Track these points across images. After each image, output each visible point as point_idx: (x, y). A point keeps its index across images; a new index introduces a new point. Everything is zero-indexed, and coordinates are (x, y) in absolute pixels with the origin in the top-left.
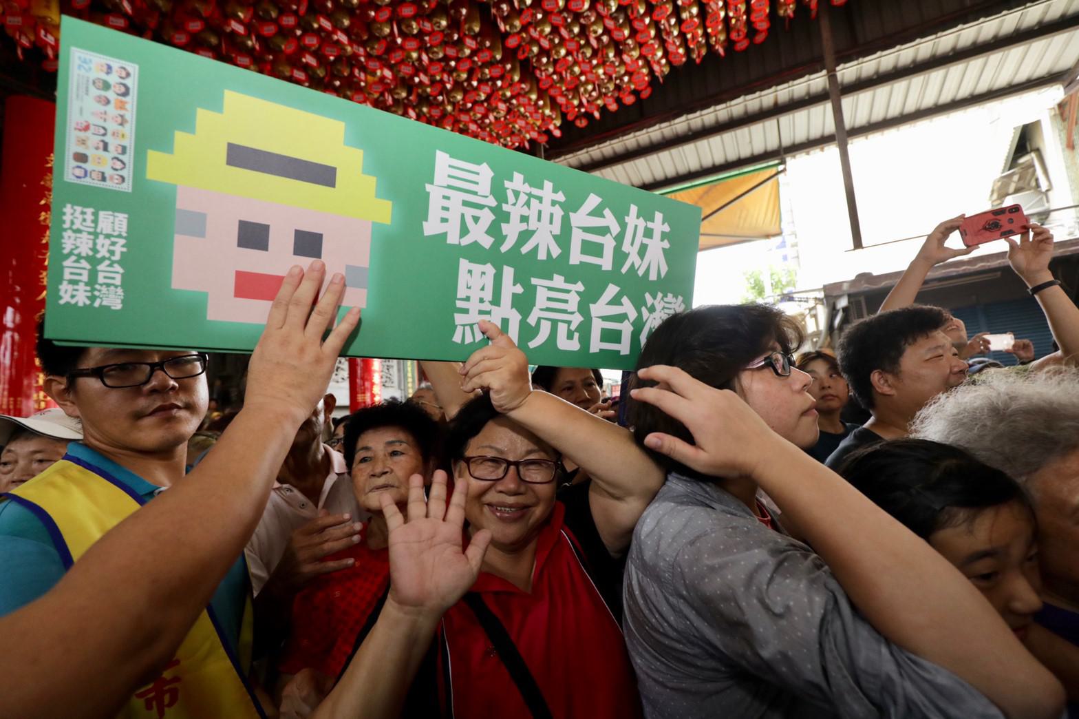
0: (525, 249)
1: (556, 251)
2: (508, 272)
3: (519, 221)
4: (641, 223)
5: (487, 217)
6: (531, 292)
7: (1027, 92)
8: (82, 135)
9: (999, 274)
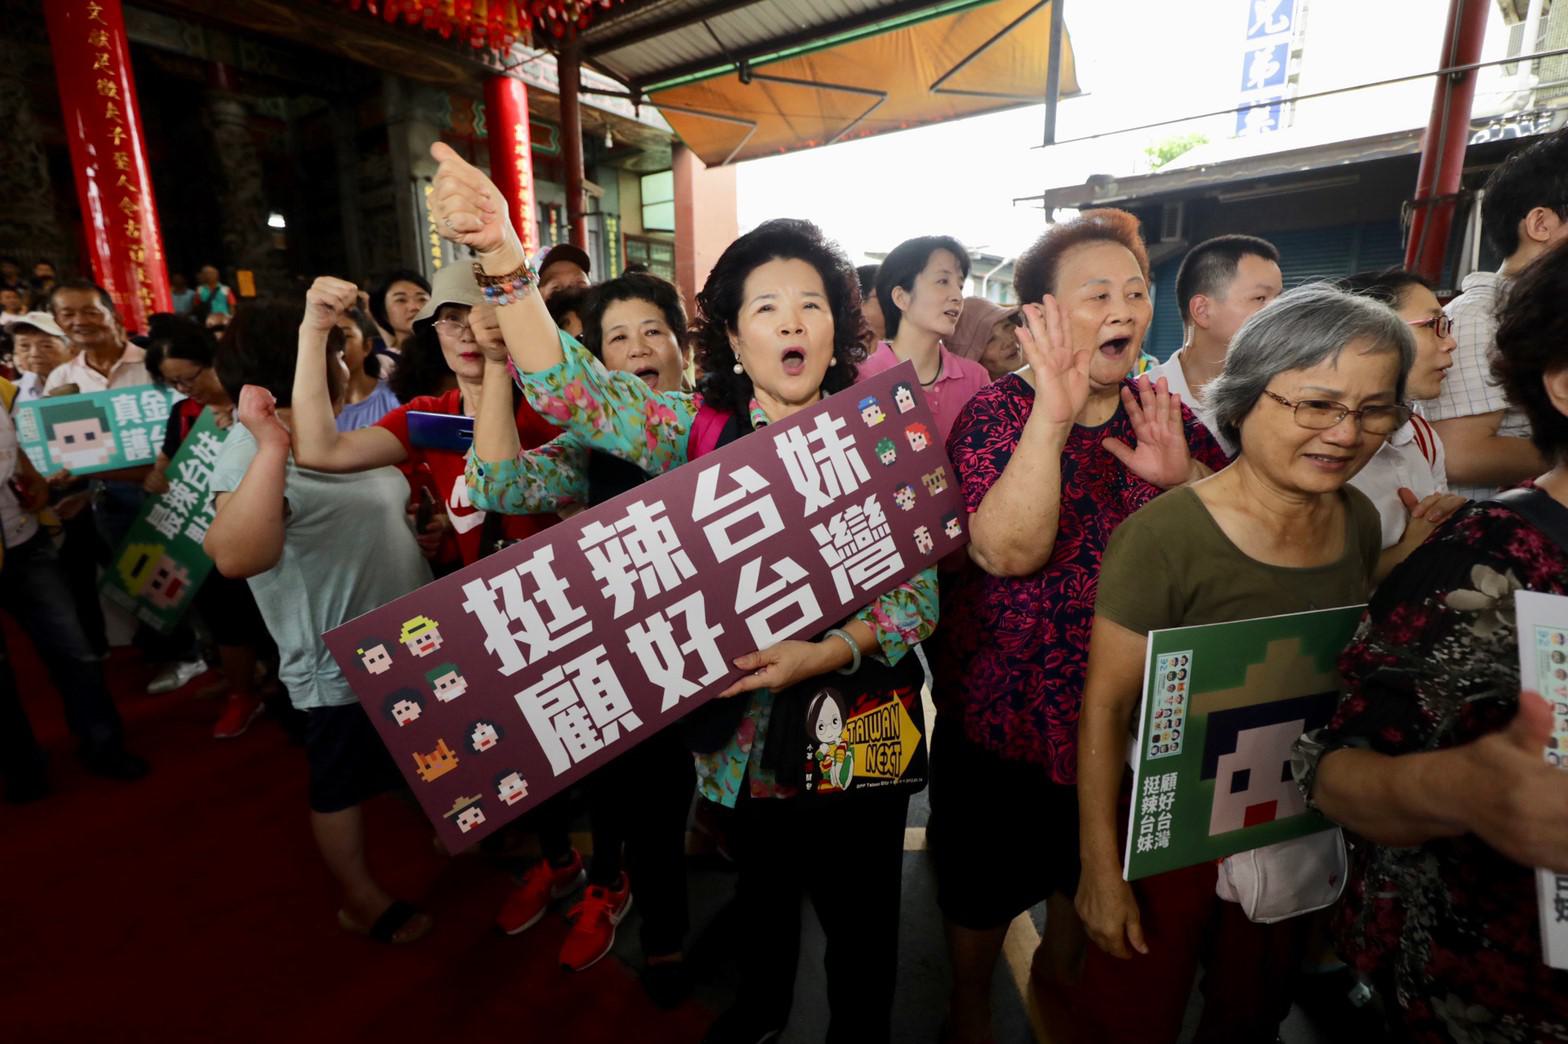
0: (190, 507)
1: (196, 495)
2: (196, 519)
3: (522, 599)
4: (200, 447)
5: (173, 515)
6: (207, 515)
7: (1482, 42)
8: (1158, 720)
9: (1357, 177)
